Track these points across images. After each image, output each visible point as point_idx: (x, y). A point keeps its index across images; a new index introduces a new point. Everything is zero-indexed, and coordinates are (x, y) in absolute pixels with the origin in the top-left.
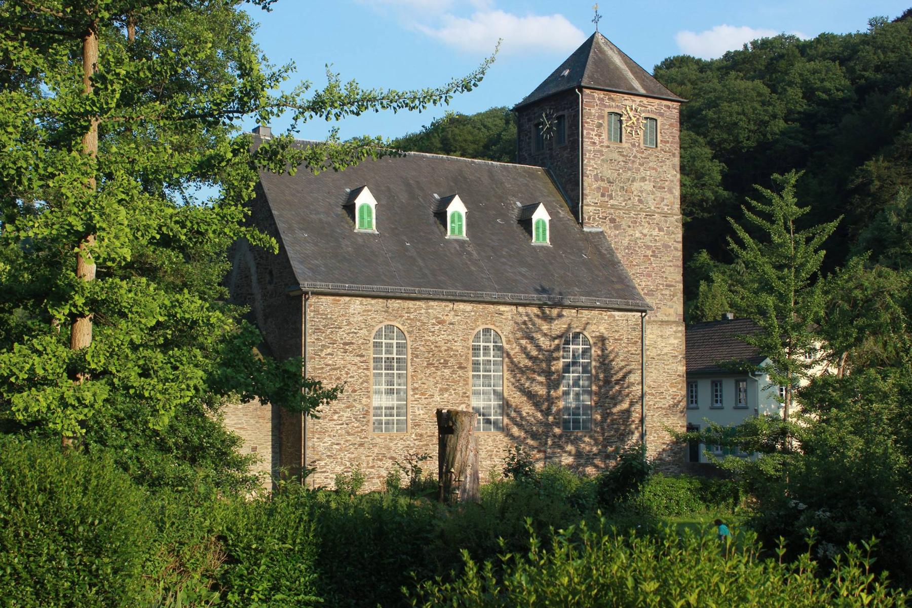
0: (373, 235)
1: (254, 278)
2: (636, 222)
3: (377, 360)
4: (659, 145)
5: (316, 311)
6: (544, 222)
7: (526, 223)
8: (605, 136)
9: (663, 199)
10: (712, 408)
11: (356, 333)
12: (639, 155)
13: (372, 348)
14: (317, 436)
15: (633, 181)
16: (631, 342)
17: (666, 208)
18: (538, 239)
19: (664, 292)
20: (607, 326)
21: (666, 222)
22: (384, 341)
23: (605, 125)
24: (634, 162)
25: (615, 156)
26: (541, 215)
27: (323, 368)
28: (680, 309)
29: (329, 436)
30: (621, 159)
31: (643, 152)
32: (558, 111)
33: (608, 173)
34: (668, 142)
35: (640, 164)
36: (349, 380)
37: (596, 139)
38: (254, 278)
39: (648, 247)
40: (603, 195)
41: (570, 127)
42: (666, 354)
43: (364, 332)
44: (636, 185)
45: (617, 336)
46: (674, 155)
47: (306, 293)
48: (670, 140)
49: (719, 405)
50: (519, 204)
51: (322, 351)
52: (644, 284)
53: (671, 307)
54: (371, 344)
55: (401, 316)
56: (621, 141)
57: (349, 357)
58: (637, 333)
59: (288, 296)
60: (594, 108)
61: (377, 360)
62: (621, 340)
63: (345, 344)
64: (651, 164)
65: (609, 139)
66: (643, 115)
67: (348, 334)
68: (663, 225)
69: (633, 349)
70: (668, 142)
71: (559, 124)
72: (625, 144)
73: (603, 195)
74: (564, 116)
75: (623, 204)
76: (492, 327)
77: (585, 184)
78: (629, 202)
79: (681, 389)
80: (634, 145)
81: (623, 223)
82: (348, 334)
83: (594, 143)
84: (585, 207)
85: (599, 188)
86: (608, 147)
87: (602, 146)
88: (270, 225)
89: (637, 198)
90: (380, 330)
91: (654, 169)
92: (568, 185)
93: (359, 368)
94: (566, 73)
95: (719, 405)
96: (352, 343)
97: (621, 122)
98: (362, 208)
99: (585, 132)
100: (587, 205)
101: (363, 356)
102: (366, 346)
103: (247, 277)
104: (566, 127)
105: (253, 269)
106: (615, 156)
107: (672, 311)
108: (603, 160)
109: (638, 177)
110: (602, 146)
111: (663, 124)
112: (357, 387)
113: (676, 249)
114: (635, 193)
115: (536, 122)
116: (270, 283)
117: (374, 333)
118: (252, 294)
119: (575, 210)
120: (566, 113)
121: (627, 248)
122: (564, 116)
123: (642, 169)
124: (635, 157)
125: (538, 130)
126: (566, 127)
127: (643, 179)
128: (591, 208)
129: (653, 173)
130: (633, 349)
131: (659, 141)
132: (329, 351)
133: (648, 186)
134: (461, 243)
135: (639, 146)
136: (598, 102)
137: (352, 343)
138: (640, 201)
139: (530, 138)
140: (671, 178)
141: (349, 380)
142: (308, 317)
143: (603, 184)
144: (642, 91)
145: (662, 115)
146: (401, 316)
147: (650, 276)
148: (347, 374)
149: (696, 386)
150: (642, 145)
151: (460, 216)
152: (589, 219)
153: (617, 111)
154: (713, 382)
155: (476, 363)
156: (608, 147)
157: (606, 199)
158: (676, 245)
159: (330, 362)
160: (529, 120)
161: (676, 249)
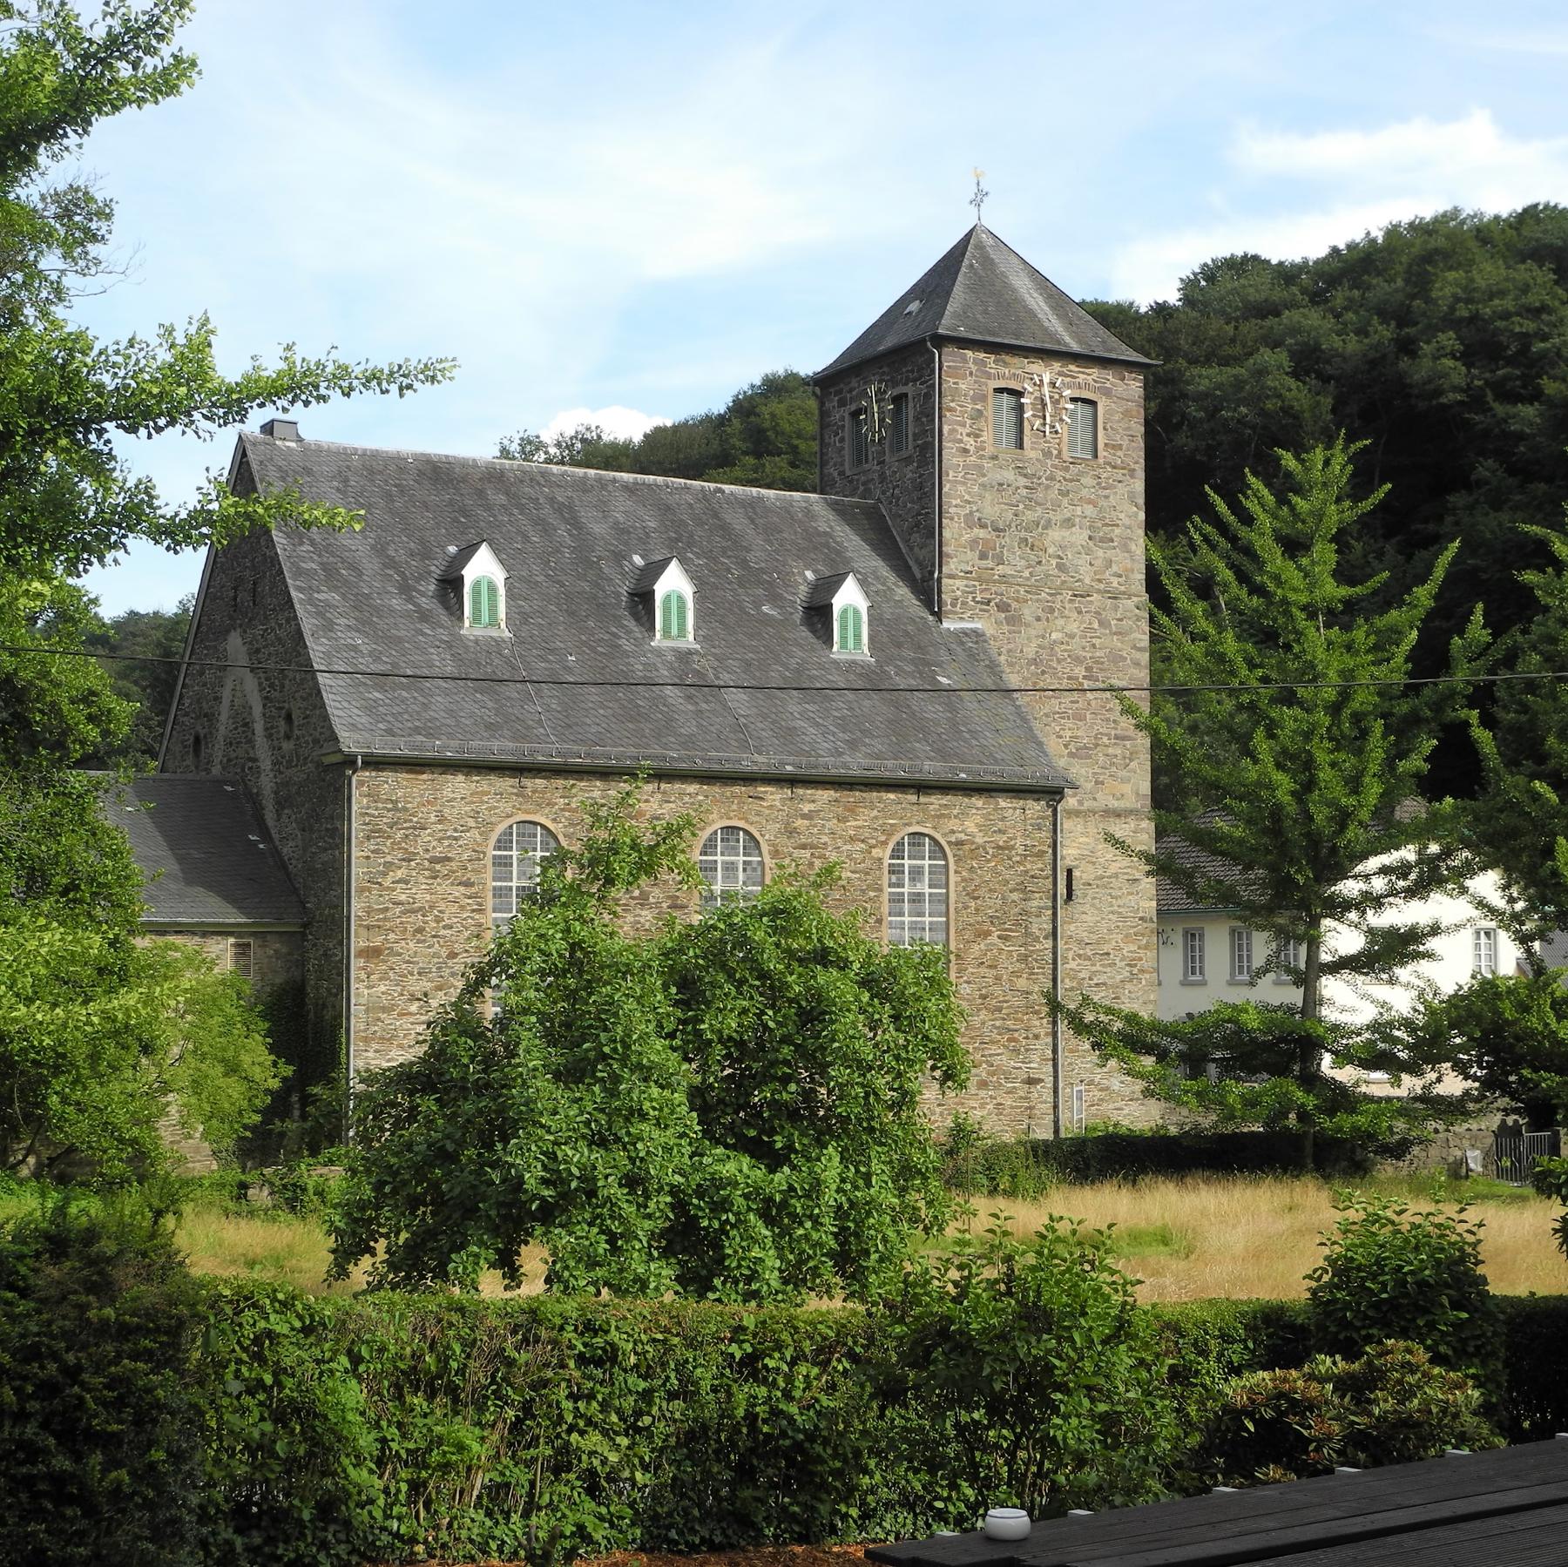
0: (498, 642)
1: (259, 727)
2: (1052, 610)
3: (498, 892)
4: (1101, 453)
5: (373, 796)
6: (856, 612)
7: (818, 614)
8: (987, 436)
9: (1109, 563)
10: (1185, 983)
11: (456, 839)
12: (1059, 474)
13: (490, 869)
14: (375, 1046)
15: (1045, 528)
16: (1032, 853)
17: (1115, 581)
18: (844, 645)
19: (1110, 751)
20: (979, 820)
21: (1116, 608)
22: (719, 858)
23: (989, 413)
24: (1048, 487)
25: (1009, 475)
26: (849, 597)
27: (387, 909)
28: (1145, 787)
29: (401, 1046)
30: (1022, 481)
31: (1067, 469)
32: (895, 384)
33: (991, 509)
34: (1120, 447)
35: (1061, 492)
36: (443, 932)
37: (970, 443)
38: (259, 727)
39: (1078, 660)
40: (983, 556)
41: (917, 419)
42: (1116, 876)
43: (475, 834)
44: (1055, 534)
45: (1001, 840)
46: (1132, 472)
47: (350, 761)
48: (1125, 443)
49: (1197, 977)
50: (809, 575)
51: (385, 874)
52: (1069, 734)
53: (1124, 781)
54: (489, 861)
55: (551, 804)
56: (1020, 446)
57: (443, 887)
58: (1046, 835)
59: (319, 764)
60: (964, 381)
61: (498, 892)
62: (1013, 848)
63: (433, 860)
64: (1084, 492)
65: (997, 441)
66: (1067, 393)
67: (440, 840)
68: (1109, 615)
69: (1035, 866)
70: (1120, 447)
71: (897, 413)
72: (1030, 452)
73: (983, 556)
74: (906, 395)
75: (1026, 574)
76: (741, 824)
77: (946, 534)
78: (1039, 568)
79: (1146, 947)
80: (1047, 454)
81: (1026, 611)
82: (440, 840)
83: (966, 451)
84: (945, 581)
85: (974, 542)
86: (995, 458)
87: (982, 457)
88: (288, 620)
89: (1054, 562)
90: (900, 844)
91: (1090, 502)
92: (906, 539)
93: (462, 908)
94: (914, 307)
95: (1197, 977)
96: (449, 859)
97: (1020, 409)
98: (477, 586)
99: (946, 429)
100: (951, 577)
101: (472, 885)
102: (476, 865)
103: (246, 725)
104: (911, 418)
105: (257, 710)
106: (1009, 475)
107: (1127, 788)
108: (983, 485)
109: (1056, 517)
110: (982, 457)
111: (1108, 412)
112: (458, 948)
113: (1137, 664)
114: (1050, 551)
115: (853, 407)
116: (288, 737)
117: (494, 837)
118: (255, 760)
119: (927, 591)
120: (909, 389)
121: (1034, 662)
122: (906, 395)
123: (1065, 502)
124: (1051, 478)
125: (858, 423)
126: (911, 418)
127: (1068, 523)
128: (958, 583)
129: (1090, 510)
130: (1035, 866)
131: (1101, 446)
132: (400, 874)
133: (1079, 536)
134: (684, 656)
135: (1059, 456)
136: (974, 368)
137: (449, 859)
138: (1060, 567)
139: (842, 440)
140: (1127, 521)
141: (443, 932)
142: (354, 808)
143: (982, 533)
144: (1075, 347)
145: (1107, 393)
146: (551, 804)
147: (1082, 718)
148: (438, 920)
149: (1202, 936)
150: (1066, 455)
151: (492, 589)
152: (954, 605)
153: (1013, 385)
154: (1233, 931)
155: (897, 899)
156: (995, 458)
157: (989, 563)
158: (1138, 655)
159: (403, 897)
160: (842, 403)
161: (1137, 664)
